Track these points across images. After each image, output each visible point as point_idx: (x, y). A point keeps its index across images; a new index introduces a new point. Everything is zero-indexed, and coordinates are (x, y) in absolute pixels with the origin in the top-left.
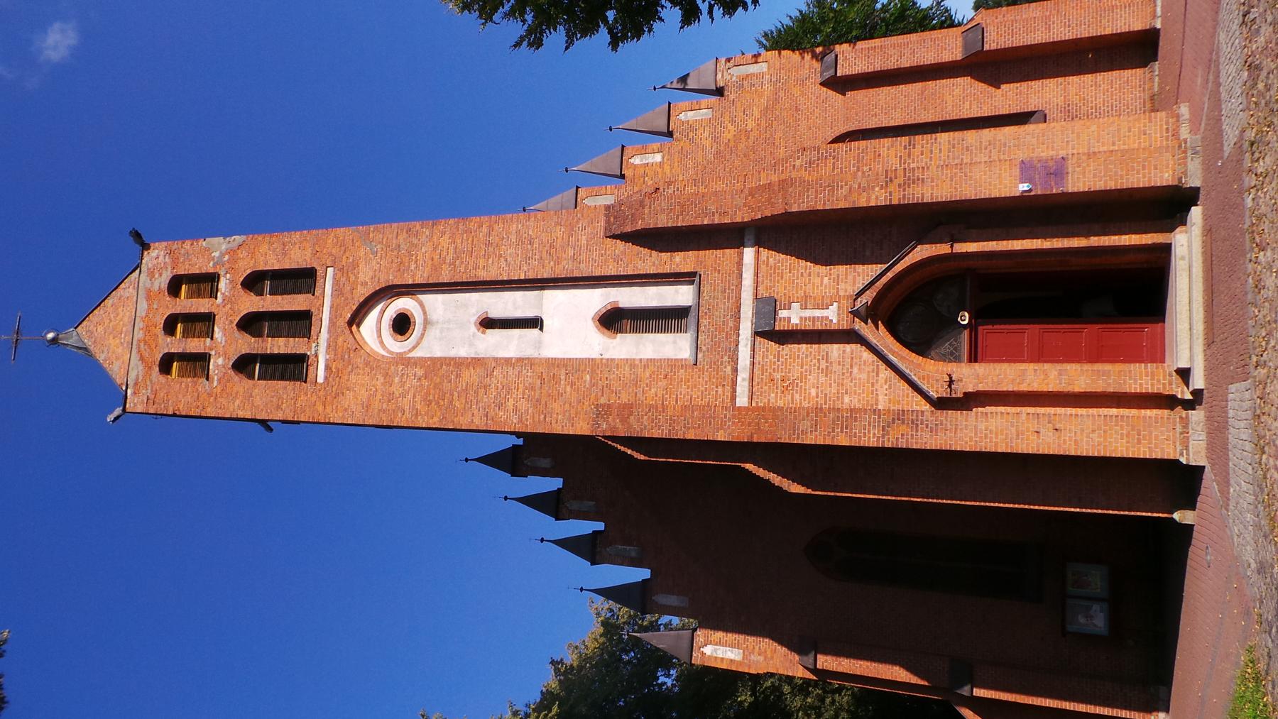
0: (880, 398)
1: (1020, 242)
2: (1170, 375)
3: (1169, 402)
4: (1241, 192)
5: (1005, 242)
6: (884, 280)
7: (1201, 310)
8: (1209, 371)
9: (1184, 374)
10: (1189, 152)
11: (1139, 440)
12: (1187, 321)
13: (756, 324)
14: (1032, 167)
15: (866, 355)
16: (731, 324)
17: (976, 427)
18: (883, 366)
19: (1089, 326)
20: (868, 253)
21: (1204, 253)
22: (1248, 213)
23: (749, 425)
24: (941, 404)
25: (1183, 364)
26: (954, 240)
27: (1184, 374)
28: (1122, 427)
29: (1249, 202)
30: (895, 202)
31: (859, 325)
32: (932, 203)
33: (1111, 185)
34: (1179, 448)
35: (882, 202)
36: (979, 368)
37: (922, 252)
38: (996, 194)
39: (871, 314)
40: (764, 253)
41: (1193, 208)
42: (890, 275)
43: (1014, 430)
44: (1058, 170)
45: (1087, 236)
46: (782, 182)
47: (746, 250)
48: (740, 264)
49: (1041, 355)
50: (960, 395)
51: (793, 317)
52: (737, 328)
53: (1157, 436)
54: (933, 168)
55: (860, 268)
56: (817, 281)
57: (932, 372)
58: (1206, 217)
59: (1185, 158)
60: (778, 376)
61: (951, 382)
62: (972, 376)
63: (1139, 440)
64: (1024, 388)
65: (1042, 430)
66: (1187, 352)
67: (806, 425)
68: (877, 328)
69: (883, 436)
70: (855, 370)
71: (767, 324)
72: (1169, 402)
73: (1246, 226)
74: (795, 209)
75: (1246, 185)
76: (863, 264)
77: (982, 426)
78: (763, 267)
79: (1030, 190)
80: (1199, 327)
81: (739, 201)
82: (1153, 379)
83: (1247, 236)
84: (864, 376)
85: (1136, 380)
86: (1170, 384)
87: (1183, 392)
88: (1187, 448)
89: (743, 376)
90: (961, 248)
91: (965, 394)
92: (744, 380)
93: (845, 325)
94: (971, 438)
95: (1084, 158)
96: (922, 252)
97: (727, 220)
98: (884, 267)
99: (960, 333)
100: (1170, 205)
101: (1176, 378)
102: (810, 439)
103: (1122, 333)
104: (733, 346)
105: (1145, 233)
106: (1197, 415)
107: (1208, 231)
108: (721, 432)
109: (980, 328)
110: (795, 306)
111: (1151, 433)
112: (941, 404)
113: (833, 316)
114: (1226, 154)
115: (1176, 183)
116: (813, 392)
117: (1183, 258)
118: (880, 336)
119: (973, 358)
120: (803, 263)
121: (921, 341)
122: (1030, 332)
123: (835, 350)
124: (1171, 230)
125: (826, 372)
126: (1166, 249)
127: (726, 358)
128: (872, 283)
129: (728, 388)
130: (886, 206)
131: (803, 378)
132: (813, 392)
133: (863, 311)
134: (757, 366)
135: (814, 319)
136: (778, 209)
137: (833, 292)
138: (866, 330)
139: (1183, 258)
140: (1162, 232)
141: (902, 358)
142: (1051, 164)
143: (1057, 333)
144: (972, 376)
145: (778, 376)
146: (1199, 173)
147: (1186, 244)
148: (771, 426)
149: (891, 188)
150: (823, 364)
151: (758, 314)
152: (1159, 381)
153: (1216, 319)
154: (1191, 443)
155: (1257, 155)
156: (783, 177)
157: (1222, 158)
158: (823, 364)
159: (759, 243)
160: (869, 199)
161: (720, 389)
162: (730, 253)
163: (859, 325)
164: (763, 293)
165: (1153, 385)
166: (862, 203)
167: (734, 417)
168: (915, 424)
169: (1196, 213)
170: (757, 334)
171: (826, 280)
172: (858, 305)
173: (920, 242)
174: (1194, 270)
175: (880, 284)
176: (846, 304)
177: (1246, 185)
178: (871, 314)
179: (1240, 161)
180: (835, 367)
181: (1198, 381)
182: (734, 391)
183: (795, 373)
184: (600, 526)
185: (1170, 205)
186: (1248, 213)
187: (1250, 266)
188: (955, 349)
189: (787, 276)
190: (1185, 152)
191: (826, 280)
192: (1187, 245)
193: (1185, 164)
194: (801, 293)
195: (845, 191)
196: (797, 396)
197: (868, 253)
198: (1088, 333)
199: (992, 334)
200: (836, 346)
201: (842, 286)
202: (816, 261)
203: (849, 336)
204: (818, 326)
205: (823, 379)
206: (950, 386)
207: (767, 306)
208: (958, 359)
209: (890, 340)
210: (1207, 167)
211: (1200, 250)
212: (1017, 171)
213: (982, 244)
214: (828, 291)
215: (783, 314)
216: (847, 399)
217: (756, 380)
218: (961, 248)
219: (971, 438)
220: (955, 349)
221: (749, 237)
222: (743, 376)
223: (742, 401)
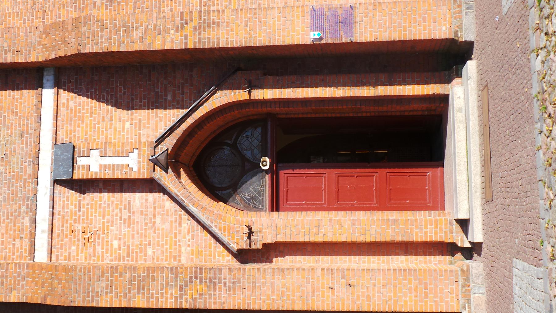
0: (183, 249)
1: (314, 89)
2: (451, 224)
3: (451, 249)
4: (526, 51)
5: (300, 90)
6: (185, 126)
7: (479, 164)
8: (488, 228)
9: (464, 224)
10: (464, 6)
11: (426, 294)
12: (465, 172)
13: (54, 171)
14: (322, 15)
15: (169, 204)
16: (29, 171)
17: (273, 284)
18: (185, 216)
19: (378, 170)
20: (169, 98)
21: (481, 108)
22: (535, 77)
23: (43, 283)
24: (243, 256)
25: (462, 216)
26: (252, 86)
27: (464, 224)
28: (410, 281)
29: (537, 64)
30: (190, 46)
31: (160, 175)
32: (228, 48)
33: (395, 36)
34: (462, 301)
35: (177, 46)
36: (279, 217)
37: (222, 98)
38: (289, 41)
39: (173, 162)
40: (64, 95)
41: (468, 62)
42: (190, 121)
43: (309, 286)
44: (347, 19)
45: (375, 84)
46: (76, 20)
47: (45, 91)
48: (39, 107)
49: (337, 202)
50: (259, 246)
51: (92, 165)
52: (36, 176)
53: (442, 289)
54: (228, 12)
55: (162, 113)
56: (119, 126)
57: (233, 221)
58: (482, 72)
59: (460, 12)
60: (79, 227)
61: (250, 234)
62: (273, 226)
63: (426, 294)
64: (320, 238)
65: (336, 286)
66: (466, 202)
67: (101, 285)
68: (178, 176)
69: (181, 296)
70: (158, 220)
71: (66, 173)
72: (451, 249)
73: (534, 92)
74: (88, 49)
75: (533, 44)
76: (165, 108)
77: (279, 283)
78: (62, 110)
79: (321, 39)
80: (477, 180)
81: (34, 39)
82: (436, 227)
83: (536, 105)
84: (166, 226)
85: (421, 229)
86: (452, 232)
87: (462, 241)
88: (469, 301)
89: (43, 225)
90: (259, 94)
91: (264, 245)
92: (43, 232)
93: (145, 174)
94: (268, 296)
95: (371, 8)
96: (222, 98)
97: (20, 59)
98: (185, 111)
99: (263, 178)
100: (447, 58)
101: (457, 227)
102: (104, 302)
103: (408, 177)
104: (31, 195)
105: (427, 83)
106: (476, 265)
107: (484, 88)
108: (14, 293)
109: (281, 173)
110: (95, 153)
111: (436, 285)
112: (243, 256)
113: (135, 165)
114: (505, 10)
115: (452, 36)
116: (116, 243)
117: (460, 110)
118: (183, 186)
119: (275, 206)
120: (104, 106)
121: (219, 188)
122: (326, 177)
123: (137, 198)
124: (449, 81)
125: (129, 222)
126: (444, 99)
127: (24, 208)
128: (172, 130)
129: (26, 241)
130: (181, 50)
131: (105, 229)
132: (116, 243)
133: (162, 159)
134: (56, 217)
135: (114, 167)
136: (71, 50)
137: (135, 138)
138: (166, 178)
139: (460, 110)
140: (440, 83)
141: (203, 209)
142: (340, 12)
143: (351, 178)
144: (273, 226)
145: (79, 227)
146: (473, 28)
147: (462, 96)
148: (64, 287)
149: (188, 31)
150: (126, 214)
151: (56, 160)
152: (441, 229)
153: (495, 180)
154: (473, 295)
155: (547, 11)
156: (83, 14)
157: (499, 13)
158: (126, 214)
159: (58, 85)
160: (164, 42)
161: (18, 242)
162: (28, 95)
163: (160, 175)
164: (63, 138)
165: (436, 233)
166: (158, 46)
167: (28, 275)
168: (212, 283)
169: (471, 67)
170: (57, 182)
171: (127, 125)
172: (159, 151)
173: (219, 87)
174: (471, 124)
175: (180, 131)
176: (147, 151)
177: (533, 44)
178: (173, 162)
179: (524, 18)
180: (138, 217)
181: (477, 234)
182: (33, 244)
183: (97, 224)
184: (182, 170)
185: (447, 58)
186: (535, 77)
187: (541, 139)
188: (259, 193)
189: (88, 120)
190: (460, 6)
191: (127, 125)
192: (463, 96)
193: (461, 18)
194: (102, 139)
195: (140, 32)
196: (99, 249)
197: (169, 98)
198: (378, 176)
199: (293, 178)
200: (138, 195)
201: (144, 131)
202: (117, 105)
203: (150, 185)
204: (119, 175)
205: (125, 230)
206: (249, 237)
207: (68, 153)
208: (258, 208)
209: (193, 188)
210: (482, 23)
211: (476, 104)
212: (308, 19)
213: (278, 91)
214: (129, 136)
215: (81, 161)
216: (150, 251)
217: (56, 231)
218: (259, 94)
219: (268, 296)
220: (259, 193)
221: (48, 78)
222: (43, 225)
223: (41, 256)
